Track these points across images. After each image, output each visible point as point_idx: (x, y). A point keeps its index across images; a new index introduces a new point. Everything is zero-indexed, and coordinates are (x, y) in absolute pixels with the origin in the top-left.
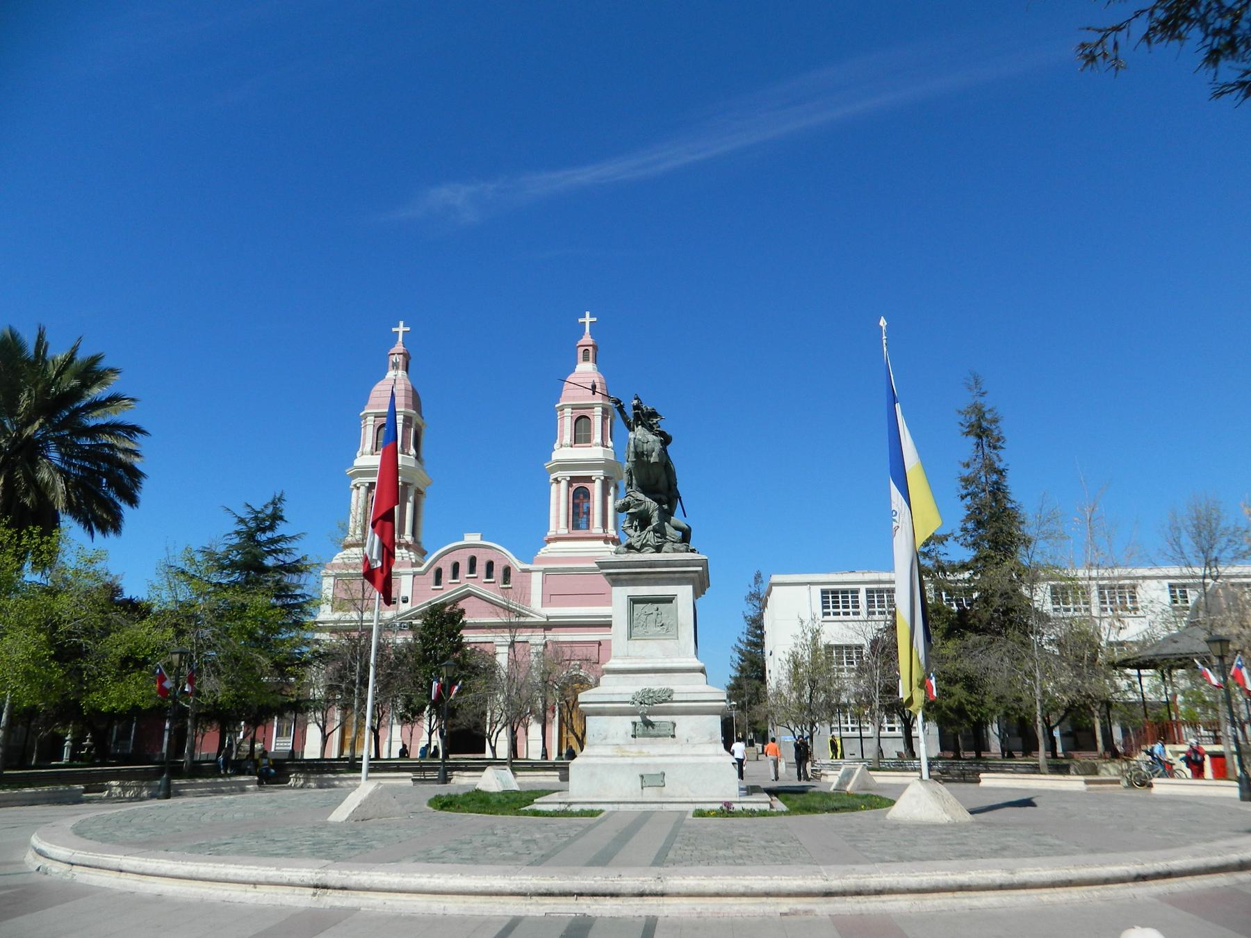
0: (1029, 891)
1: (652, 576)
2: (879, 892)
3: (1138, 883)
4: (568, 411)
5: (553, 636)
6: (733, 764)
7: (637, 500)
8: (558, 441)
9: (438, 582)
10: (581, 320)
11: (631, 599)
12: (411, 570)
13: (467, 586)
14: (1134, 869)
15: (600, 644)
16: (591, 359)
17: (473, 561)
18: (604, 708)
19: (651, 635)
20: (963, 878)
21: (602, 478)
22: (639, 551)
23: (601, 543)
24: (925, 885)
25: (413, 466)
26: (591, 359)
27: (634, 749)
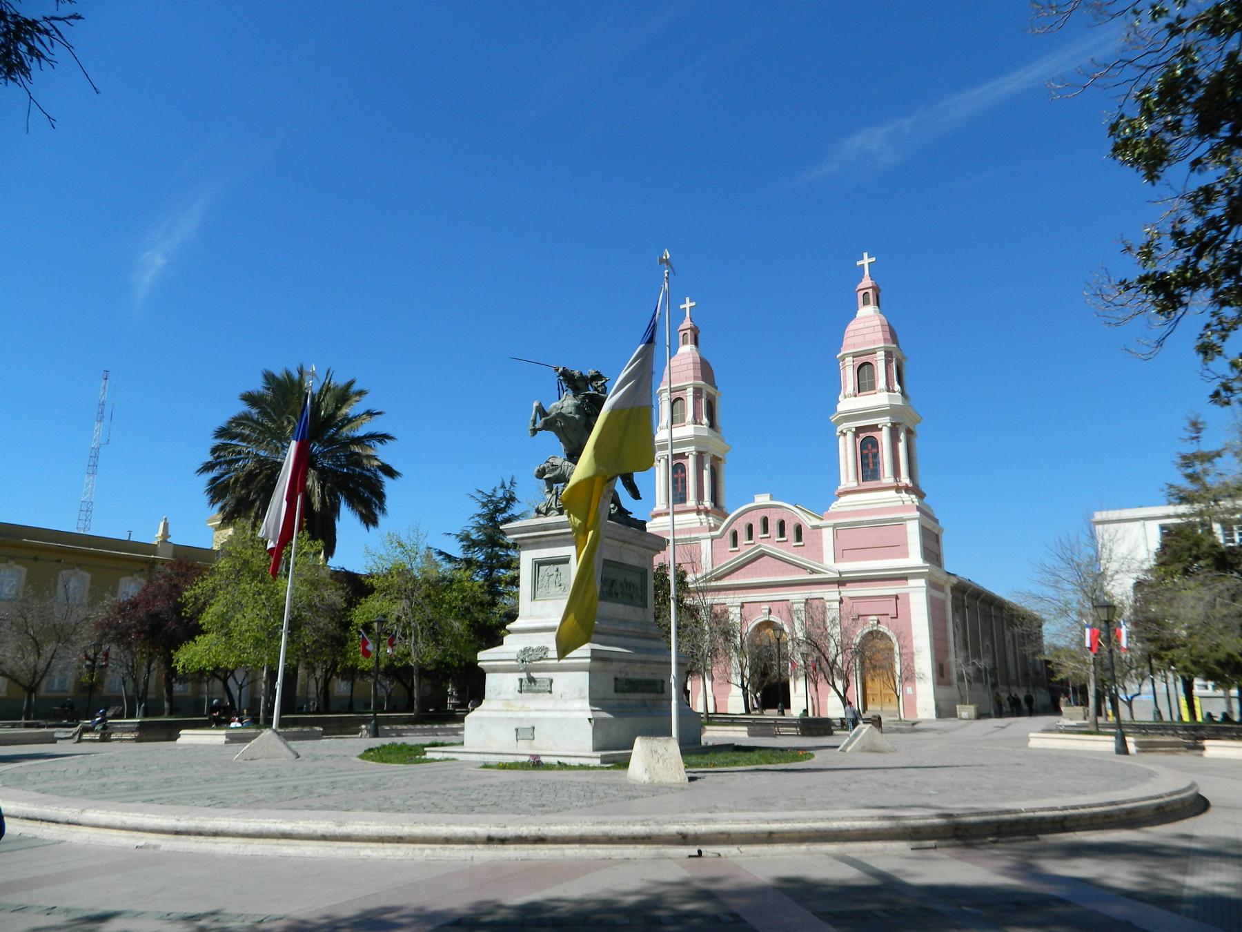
0: (354, 844)
1: (549, 538)
2: (216, 834)
3: (492, 846)
4: (849, 360)
5: (850, 591)
6: (590, 719)
7: (553, 465)
8: (842, 392)
9: (735, 544)
10: (859, 263)
11: (536, 563)
12: (708, 534)
13: (759, 546)
14: (482, 830)
15: (897, 597)
16: (872, 302)
17: (765, 521)
18: (496, 666)
19: (552, 596)
20: (286, 827)
21: (889, 425)
22: (546, 514)
23: (892, 493)
24: (250, 831)
25: (706, 434)
26: (872, 302)
27: (519, 704)
